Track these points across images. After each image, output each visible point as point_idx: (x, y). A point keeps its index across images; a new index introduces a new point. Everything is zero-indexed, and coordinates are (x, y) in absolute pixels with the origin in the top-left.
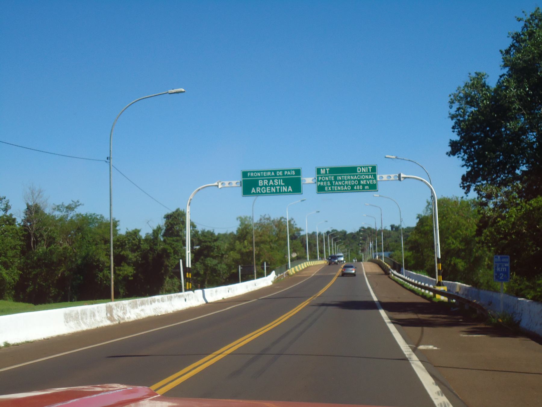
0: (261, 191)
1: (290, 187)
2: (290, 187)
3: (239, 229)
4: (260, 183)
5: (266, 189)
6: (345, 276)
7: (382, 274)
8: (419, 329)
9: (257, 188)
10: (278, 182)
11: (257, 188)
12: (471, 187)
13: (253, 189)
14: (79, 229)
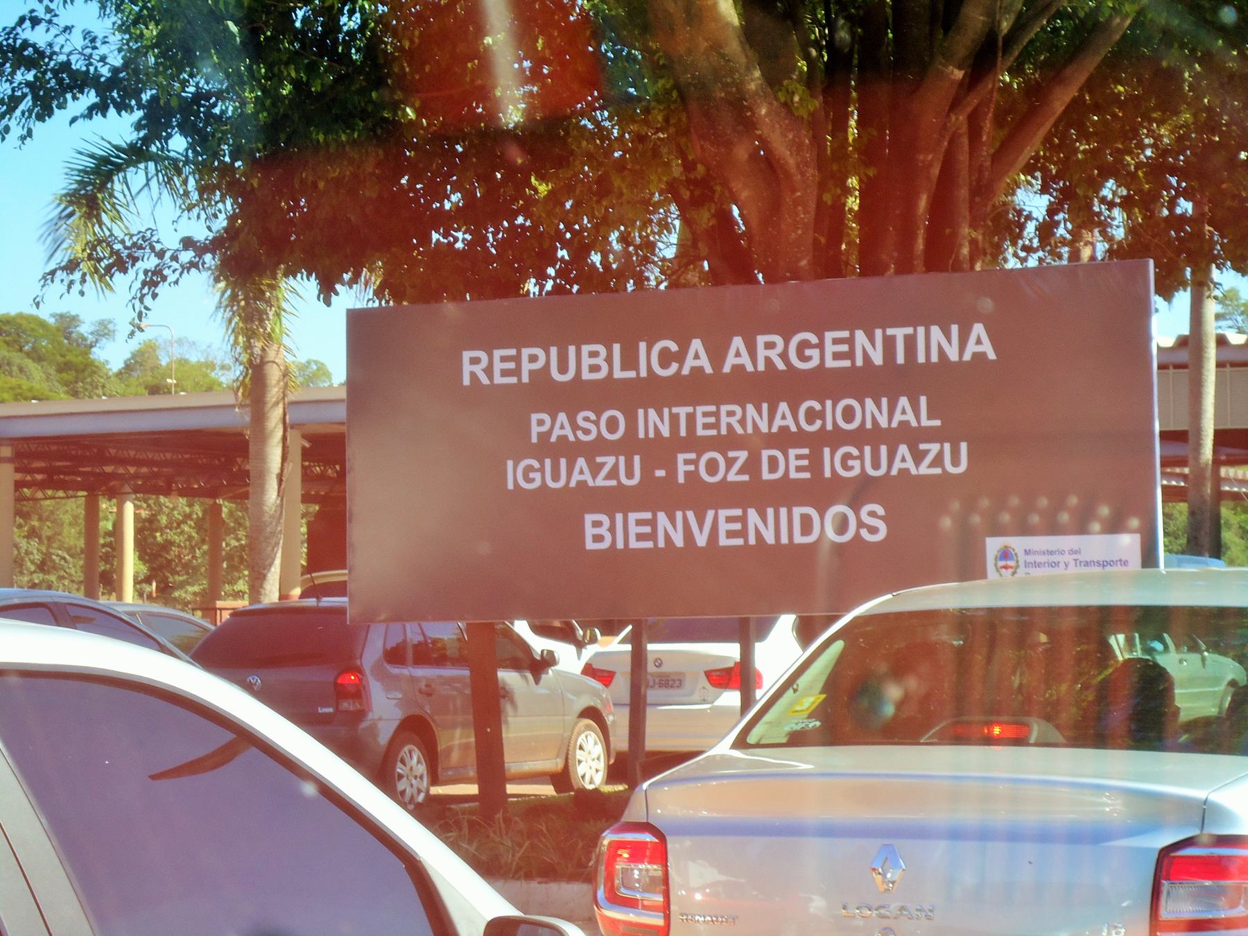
0: (784, 356)
1: (978, 329)
2: (978, 329)
3: (949, 610)
4: (590, 531)
5: (821, 346)
6: (605, 671)
7: (760, 740)
8: (627, 699)
9: (761, 340)
10: (612, 530)
11: (761, 340)
12: (373, 627)
13: (738, 342)
14: (260, 476)
